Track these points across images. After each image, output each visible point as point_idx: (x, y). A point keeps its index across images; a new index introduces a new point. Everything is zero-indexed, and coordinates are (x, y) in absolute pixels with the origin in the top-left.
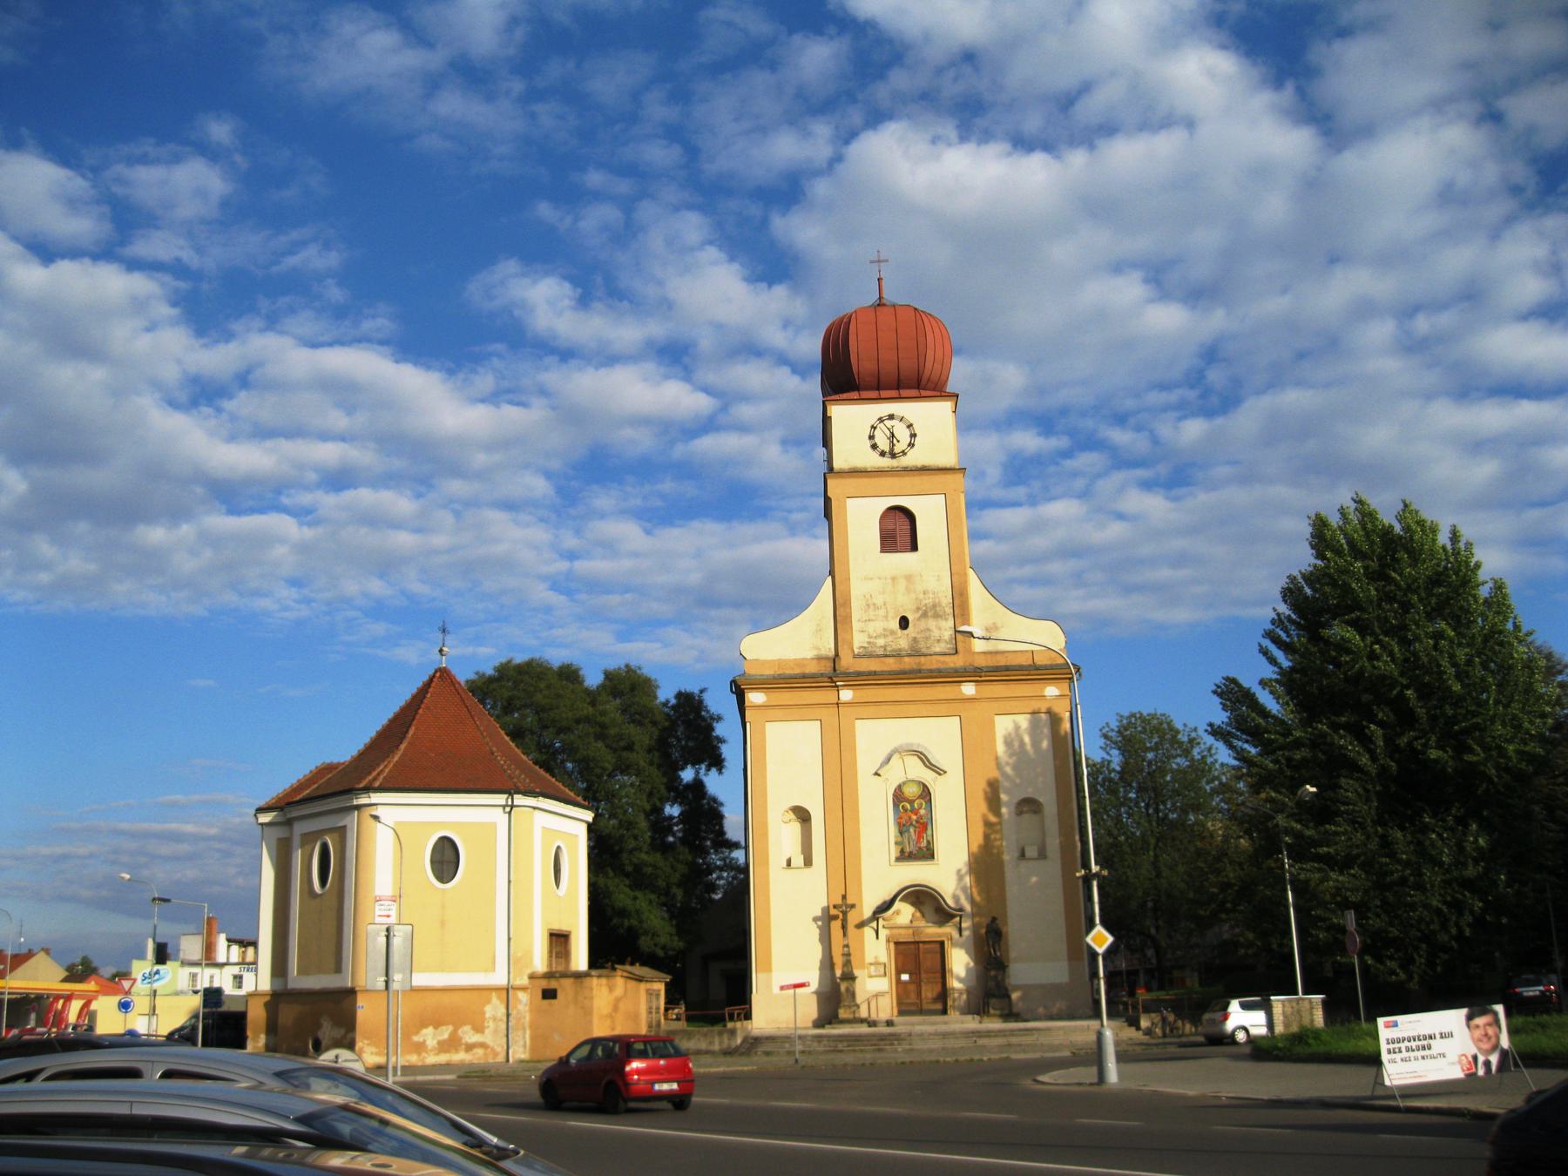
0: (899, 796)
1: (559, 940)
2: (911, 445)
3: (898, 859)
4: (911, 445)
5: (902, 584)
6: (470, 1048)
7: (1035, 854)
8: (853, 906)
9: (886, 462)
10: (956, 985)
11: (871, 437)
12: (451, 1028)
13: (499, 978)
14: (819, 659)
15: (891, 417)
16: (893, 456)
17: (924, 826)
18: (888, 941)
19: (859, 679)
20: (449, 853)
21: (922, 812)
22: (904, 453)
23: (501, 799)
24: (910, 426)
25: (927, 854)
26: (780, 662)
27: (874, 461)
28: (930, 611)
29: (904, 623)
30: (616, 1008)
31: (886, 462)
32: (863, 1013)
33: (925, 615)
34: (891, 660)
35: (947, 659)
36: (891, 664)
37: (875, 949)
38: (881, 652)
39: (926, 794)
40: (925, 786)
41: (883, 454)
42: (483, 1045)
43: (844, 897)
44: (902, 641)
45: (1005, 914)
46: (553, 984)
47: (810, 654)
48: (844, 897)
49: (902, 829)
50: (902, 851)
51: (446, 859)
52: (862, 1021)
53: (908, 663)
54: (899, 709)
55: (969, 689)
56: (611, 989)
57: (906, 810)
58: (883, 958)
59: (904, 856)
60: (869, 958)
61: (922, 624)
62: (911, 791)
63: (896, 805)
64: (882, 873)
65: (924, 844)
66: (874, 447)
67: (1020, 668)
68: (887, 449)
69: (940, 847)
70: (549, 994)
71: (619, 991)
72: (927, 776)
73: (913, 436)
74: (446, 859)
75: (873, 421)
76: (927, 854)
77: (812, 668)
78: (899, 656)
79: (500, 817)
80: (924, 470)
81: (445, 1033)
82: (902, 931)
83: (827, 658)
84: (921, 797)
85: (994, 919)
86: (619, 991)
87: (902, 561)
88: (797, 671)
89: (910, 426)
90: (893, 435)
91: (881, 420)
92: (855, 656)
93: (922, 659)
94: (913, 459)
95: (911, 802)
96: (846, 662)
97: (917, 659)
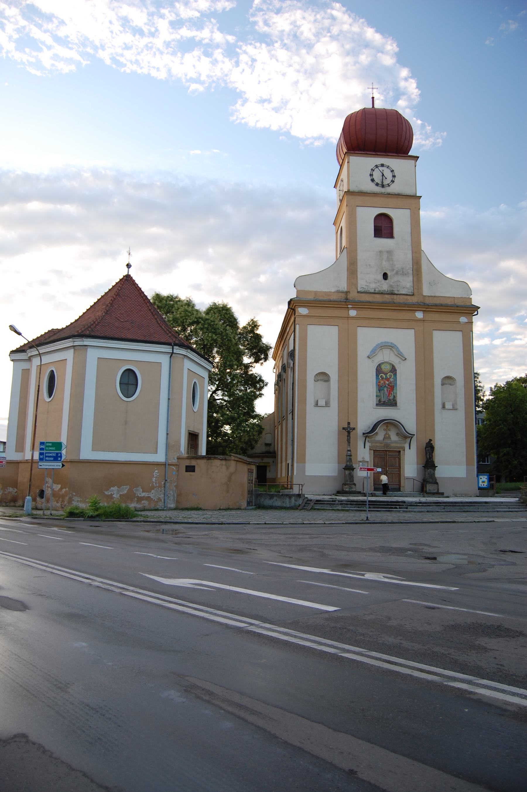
0: (379, 370)
1: (193, 437)
2: (393, 181)
3: (377, 405)
4: (393, 181)
5: (385, 256)
6: (140, 499)
7: (451, 408)
8: (354, 429)
9: (378, 189)
10: (262, 500)
11: (371, 175)
12: (128, 487)
13: (160, 457)
14: (338, 292)
15: (382, 165)
16: (383, 186)
17: (392, 387)
18: (370, 449)
19: (359, 305)
20: (132, 380)
21: (391, 380)
22: (389, 185)
23: (168, 349)
24: (392, 171)
25: (393, 403)
26: (316, 293)
27: (372, 187)
28: (401, 272)
29: (385, 276)
30: (230, 479)
31: (378, 189)
32: (359, 488)
33: (397, 273)
34: (378, 296)
35: (409, 297)
36: (378, 298)
37: (363, 453)
38: (373, 291)
39: (394, 370)
40: (393, 366)
41: (377, 184)
42: (148, 498)
43: (349, 423)
44: (385, 286)
45: (434, 438)
46: (193, 463)
47: (333, 290)
48: (349, 423)
49: (380, 388)
50: (380, 401)
51: (129, 381)
52: (359, 493)
53: (387, 298)
54: (381, 323)
55: (419, 315)
56: (227, 468)
57: (382, 378)
58: (367, 459)
59: (381, 404)
60: (360, 458)
61: (396, 279)
62: (386, 368)
63: (377, 375)
64: (367, 414)
65: (391, 398)
66: (373, 180)
67: (447, 306)
68: (380, 182)
69: (400, 400)
70: (190, 469)
71: (232, 469)
72: (395, 360)
73: (394, 176)
74: (129, 381)
75: (372, 166)
76: (393, 403)
77: (334, 297)
78: (382, 293)
79: (164, 360)
80: (398, 195)
81: (125, 490)
82: (378, 444)
83: (342, 292)
84: (391, 371)
85: (430, 440)
86: (232, 469)
87: (384, 243)
88: (326, 298)
89: (392, 171)
90: (383, 175)
91: (377, 166)
92: (358, 292)
93: (395, 297)
94: (394, 189)
95: (386, 374)
96: (351, 296)
97: (392, 296)
